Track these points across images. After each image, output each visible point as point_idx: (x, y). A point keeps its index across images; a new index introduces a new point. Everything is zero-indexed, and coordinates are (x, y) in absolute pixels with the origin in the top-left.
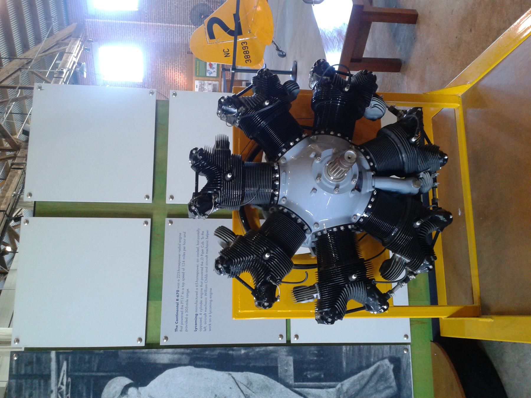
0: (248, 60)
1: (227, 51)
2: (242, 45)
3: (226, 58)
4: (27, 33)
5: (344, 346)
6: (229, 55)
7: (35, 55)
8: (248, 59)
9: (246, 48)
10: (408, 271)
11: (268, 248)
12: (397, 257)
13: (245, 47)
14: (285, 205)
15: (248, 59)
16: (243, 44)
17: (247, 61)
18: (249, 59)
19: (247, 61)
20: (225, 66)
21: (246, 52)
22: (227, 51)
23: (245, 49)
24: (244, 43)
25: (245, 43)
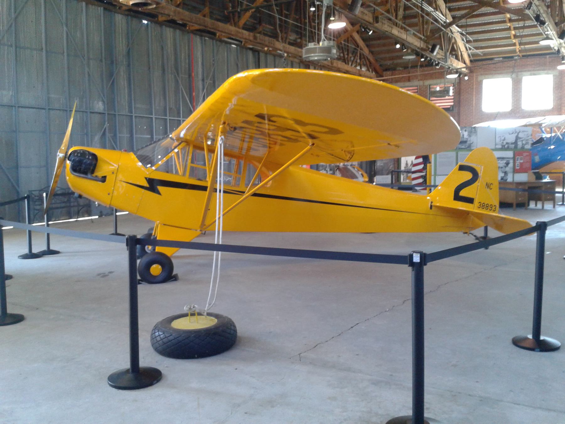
0: (480, 205)
1: (491, 188)
2: (494, 206)
3: (485, 184)
4: (453, 102)
5: (262, 169)
6: (487, 187)
7: (475, 98)
8: (481, 205)
9: (491, 209)
10: (391, 14)
11: (13, 94)
12: (275, 3)
13: (492, 207)
14: (408, 174)
15: (481, 205)
16: (495, 207)
17: (480, 204)
18: (485, 208)
19: (480, 204)
20: (225, 162)
21: (488, 207)
22: (491, 188)
23: (490, 207)
24: (495, 208)
25: (494, 210)
